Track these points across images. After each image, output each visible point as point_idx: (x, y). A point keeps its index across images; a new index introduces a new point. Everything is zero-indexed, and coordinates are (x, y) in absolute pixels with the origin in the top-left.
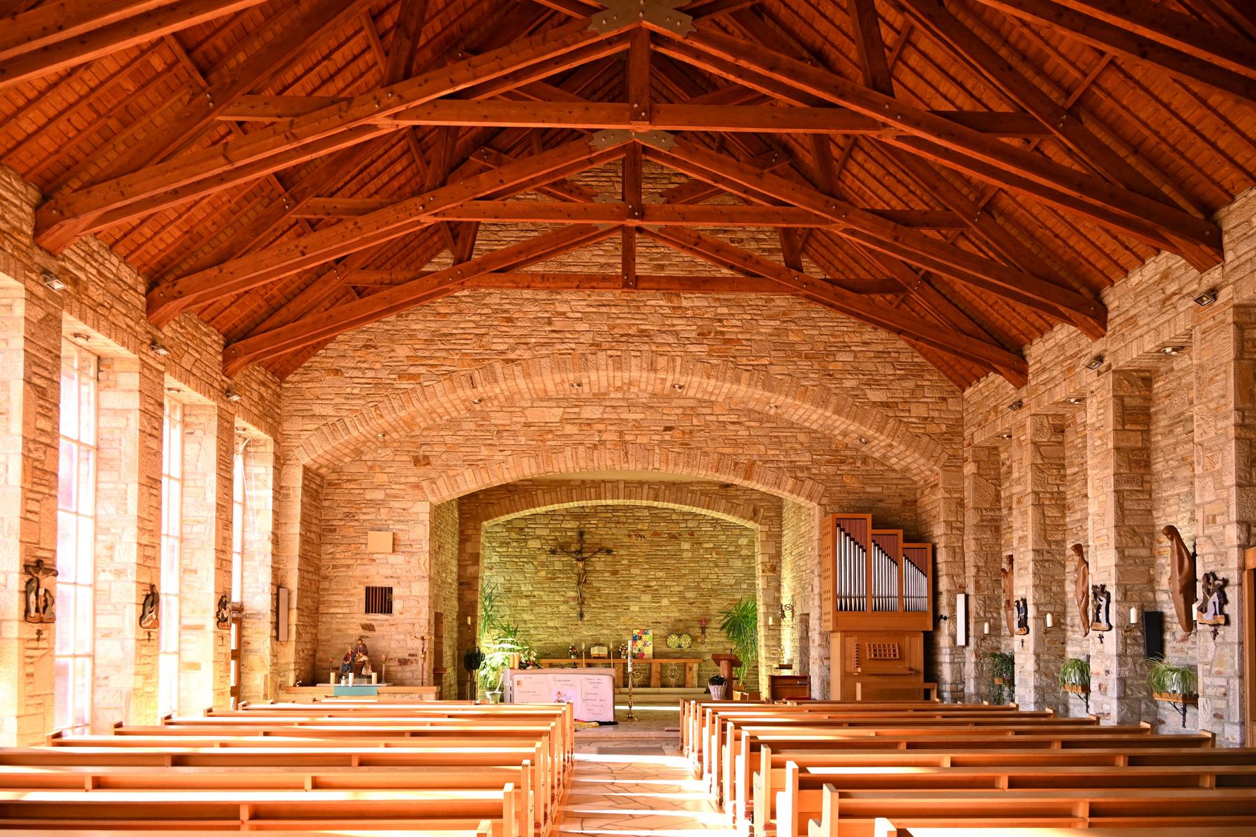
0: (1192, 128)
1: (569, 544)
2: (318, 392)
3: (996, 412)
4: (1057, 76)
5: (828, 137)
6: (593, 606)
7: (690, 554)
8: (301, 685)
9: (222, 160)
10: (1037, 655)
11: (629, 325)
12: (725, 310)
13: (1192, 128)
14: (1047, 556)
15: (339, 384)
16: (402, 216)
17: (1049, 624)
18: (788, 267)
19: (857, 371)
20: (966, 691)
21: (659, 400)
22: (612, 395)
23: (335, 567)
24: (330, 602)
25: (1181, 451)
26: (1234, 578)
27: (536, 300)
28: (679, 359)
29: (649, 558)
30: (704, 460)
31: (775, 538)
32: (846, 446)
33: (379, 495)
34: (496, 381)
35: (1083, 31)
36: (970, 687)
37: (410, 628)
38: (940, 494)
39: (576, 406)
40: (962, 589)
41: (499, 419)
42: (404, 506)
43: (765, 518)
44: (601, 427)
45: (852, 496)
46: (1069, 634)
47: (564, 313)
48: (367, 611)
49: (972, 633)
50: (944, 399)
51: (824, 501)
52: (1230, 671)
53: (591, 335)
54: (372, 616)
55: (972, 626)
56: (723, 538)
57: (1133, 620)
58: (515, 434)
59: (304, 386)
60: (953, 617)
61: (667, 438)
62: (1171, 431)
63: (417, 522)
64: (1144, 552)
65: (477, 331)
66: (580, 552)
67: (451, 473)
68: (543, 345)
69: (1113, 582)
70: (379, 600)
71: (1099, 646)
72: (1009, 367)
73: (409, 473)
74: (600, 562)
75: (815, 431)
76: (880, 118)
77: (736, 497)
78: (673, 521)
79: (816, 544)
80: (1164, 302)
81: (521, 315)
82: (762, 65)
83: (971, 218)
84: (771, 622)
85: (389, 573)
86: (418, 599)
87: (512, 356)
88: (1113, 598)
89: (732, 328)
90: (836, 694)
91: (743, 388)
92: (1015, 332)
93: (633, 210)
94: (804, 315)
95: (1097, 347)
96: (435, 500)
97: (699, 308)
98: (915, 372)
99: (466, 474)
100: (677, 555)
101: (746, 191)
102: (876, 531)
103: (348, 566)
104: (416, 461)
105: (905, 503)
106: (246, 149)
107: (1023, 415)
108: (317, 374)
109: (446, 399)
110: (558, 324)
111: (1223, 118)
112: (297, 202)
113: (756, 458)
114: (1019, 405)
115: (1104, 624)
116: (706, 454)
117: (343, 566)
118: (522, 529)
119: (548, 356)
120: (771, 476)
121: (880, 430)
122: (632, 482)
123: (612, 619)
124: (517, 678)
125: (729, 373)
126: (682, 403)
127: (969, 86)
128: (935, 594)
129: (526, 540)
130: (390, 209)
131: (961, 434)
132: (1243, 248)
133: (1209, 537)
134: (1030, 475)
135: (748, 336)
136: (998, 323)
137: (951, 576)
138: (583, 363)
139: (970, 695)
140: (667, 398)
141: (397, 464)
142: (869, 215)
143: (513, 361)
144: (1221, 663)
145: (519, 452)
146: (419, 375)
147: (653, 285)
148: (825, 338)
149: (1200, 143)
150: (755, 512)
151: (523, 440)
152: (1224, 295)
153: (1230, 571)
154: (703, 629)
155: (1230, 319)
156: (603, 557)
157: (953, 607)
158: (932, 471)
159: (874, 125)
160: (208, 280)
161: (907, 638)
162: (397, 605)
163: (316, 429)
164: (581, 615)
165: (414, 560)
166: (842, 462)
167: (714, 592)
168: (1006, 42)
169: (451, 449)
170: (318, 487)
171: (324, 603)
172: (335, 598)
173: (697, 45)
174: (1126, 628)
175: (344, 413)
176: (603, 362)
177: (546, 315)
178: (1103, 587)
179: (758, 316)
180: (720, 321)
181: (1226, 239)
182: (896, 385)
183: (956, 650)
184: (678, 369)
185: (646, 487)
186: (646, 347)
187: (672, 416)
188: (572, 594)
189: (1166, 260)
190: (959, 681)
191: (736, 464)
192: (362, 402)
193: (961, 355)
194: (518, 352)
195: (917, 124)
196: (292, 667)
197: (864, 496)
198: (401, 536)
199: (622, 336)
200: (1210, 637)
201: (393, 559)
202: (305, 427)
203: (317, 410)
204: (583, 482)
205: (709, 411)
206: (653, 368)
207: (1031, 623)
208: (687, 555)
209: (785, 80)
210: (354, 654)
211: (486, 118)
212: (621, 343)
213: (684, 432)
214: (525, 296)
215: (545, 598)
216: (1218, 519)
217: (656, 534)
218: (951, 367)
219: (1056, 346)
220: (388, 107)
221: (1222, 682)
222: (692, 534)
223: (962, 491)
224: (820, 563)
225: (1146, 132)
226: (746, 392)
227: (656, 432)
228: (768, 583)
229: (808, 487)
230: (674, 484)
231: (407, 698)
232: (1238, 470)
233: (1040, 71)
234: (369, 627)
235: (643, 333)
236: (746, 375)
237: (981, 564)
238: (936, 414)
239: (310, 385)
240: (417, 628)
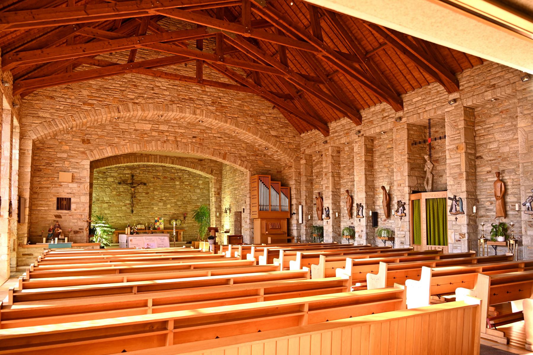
0: (401, 71)
1: (126, 180)
2: (42, 106)
3: (316, 144)
4: (365, 46)
5: (287, 48)
6: (137, 208)
7: (179, 187)
8: (30, 244)
9: (83, 12)
10: (333, 226)
11: (186, 95)
12: (222, 95)
13: (401, 71)
14: (335, 193)
15: (52, 103)
16: (129, 43)
17: (337, 216)
18: (251, 83)
19: (267, 123)
20: (302, 239)
21: (191, 125)
22: (172, 122)
23: (40, 188)
24: (38, 204)
25: (384, 163)
26: (407, 202)
27: (147, 79)
28: (205, 111)
29: (162, 187)
30: (208, 151)
31: (219, 182)
32: (259, 150)
33: (65, 155)
34: (129, 111)
35: (391, 43)
36: (303, 238)
37: (80, 217)
38: (293, 170)
39: (157, 124)
40: (300, 203)
41: (123, 126)
42: (77, 161)
43: (215, 174)
44: (167, 134)
45: (260, 168)
46: (342, 219)
47: (159, 86)
48: (58, 209)
49: (304, 219)
50: (294, 136)
51: (251, 169)
52: (406, 230)
53: (170, 97)
54: (60, 211)
55: (304, 217)
56: (193, 180)
57: (371, 214)
58: (130, 133)
59: (34, 102)
60: (298, 213)
61: (194, 141)
62: (380, 157)
63: (84, 169)
64: (372, 194)
65: (121, 89)
66: (132, 184)
67: (100, 148)
68: (150, 98)
69: (364, 202)
70: (64, 204)
71: (359, 223)
72: (324, 130)
73: (80, 146)
74: (141, 188)
75: (248, 143)
76: (320, 49)
77: (205, 165)
78: (172, 173)
79: (248, 186)
80: (383, 118)
81: (140, 84)
82: (287, 23)
83: (326, 82)
84: (218, 215)
85: (70, 191)
86: (83, 203)
87: (137, 101)
88: (364, 207)
89: (224, 101)
90: (303, 238)
91: (228, 125)
92: (326, 118)
93: (221, 58)
94: (249, 100)
95: (358, 128)
96: (92, 159)
97: (212, 92)
98: (285, 126)
99: (107, 149)
100: (174, 187)
101: (258, 58)
103: (48, 188)
104: (84, 141)
105: (278, 172)
106: (95, 10)
107: (327, 146)
108: (41, 97)
109: (104, 116)
110: (156, 91)
111: (410, 71)
112: (80, 28)
113: (227, 151)
114: (326, 142)
115: (361, 216)
116: (209, 148)
117: (45, 187)
119: (152, 103)
120: (232, 159)
121: (275, 145)
122: (163, 156)
123: (146, 213)
124: (130, 238)
125: (223, 119)
126: (200, 127)
127: (334, 41)
128: (291, 205)
129: (106, 178)
130: (124, 39)
131: (299, 149)
132: (410, 107)
133: (399, 190)
134: (330, 166)
135: (230, 106)
136: (321, 114)
137: (296, 199)
138: (167, 108)
139: (303, 241)
140: (194, 125)
141: (74, 142)
142: (298, 75)
143: (137, 103)
144: (403, 228)
145: (132, 141)
146: (94, 104)
147: (209, 84)
148: (256, 110)
149: (401, 76)
150: (212, 171)
151: (134, 136)
152: (404, 120)
153: (406, 200)
154: (185, 218)
155: (406, 127)
156: (142, 186)
157: (297, 210)
158: (289, 161)
159: (317, 50)
160: (35, 55)
162: (73, 206)
163: (40, 123)
164: (132, 211)
165: (82, 186)
166: (257, 155)
167: (189, 202)
168: (351, 33)
169: (100, 137)
170: (38, 148)
171: (34, 205)
172: (40, 202)
173: (267, 11)
174: (368, 217)
175: (55, 117)
176: (175, 109)
177: (151, 86)
178: (361, 204)
179: (234, 99)
180: (220, 98)
181: (404, 104)
182: (280, 130)
183: (298, 225)
184: (204, 115)
185: (169, 158)
186: (192, 105)
187: (196, 132)
188: (128, 202)
189: (384, 105)
190: (299, 236)
191: (220, 153)
192: (64, 113)
193: (309, 123)
194: (139, 100)
195: (330, 54)
196: (26, 235)
197: (264, 169)
198: (75, 174)
199: (183, 99)
200: (399, 220)
201: (71, 185)
202: (34, 122)
203: (41, 114)
204: (142, 154)
205: (210, 132)
206: (194, 113)
207: (331, 215)
208: (178, 187)
209: (293, 30)
210: (54, 229)
211: (193, 19)
212: (182, 102)
213: (200, 139)
214: (142, 77)
215: (115, 203)
216: (402, 185)
217: (165, 178)
218: (298, 126)
219: (341, 125)
220: (157, 7)
221: (404, 233)
222: (180, 178)
223: (300, 169)
224: (250, 193)
225: (387, 69)
226: (228, 126)
227: (190, 138)
228: (217, 199)
230: (180, 158)
231: (86, 248)
232: (408, 171)
233: (360, 44)
234: (59, 217)
235: (191, 99)
236: (229, 120)
237: (307, 195)
238: (292, 141)
239: (37, 102)
240: (83, 217)
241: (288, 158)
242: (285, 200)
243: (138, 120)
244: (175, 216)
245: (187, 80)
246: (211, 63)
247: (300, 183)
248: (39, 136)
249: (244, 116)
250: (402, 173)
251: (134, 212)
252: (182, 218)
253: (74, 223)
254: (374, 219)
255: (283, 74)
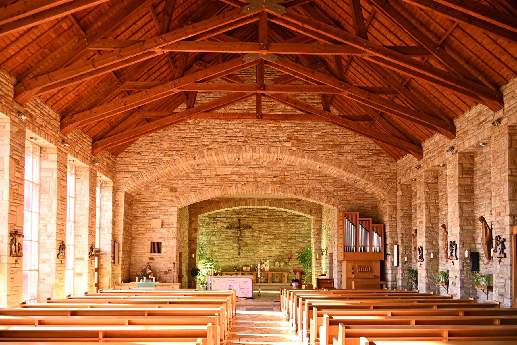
0: (491, 53)
1: (234, 224)
2: (131, 161)
3: (410, 170)
6: (244, 250)
7: (284, 229)
8: (124, 282)
10: (427, 270)
11: (259, 134)
12: (298, 128)
13: (491, 53)
14: (431, 229)
15: (139, 158)
16: (165, 89)
17: (432, 257)
18: (324, 110)
19: (353, 153)
20: (398, 285)
21: (271, 165)
22: (252, 163)
23: (138, 234)
24: (136, 248)
25: (486, 186)
26: (508, 238)
27: (221, 124)
28: (279, 148)
30: (290, 190)
31: (319, 222)
32: (348, 184)
33: (156, 204)
34: (204, 157)
35: (446, 13)
36: (399, 283)
37: (169, 259)
38: (387, 203)
39: (237, 167)
40: (396, 243)
41: (205, 173)
42: (166, 209)
43: (315, 213)
44: (248, 176)
45: (351, 205)
46: (440, 261)
47: (232, 129)
48: (151, 252)
49: (400, 261)
50: (389, 165)
51: (339, 206)
52: (506, 277)
53: (243, 138)
54: (153, 254)
55: (400, 258)
56: (298, 222)
58: (212, 179)
59: (125, 159)
60: (392, 254)
61: (275, 180)
62: (482, 178)
63: (172, 215)
64: (471, 228)
65: (196, 137)
66: (239, 227)
67: (186, 195)
68: (223, 142)
69: (458, 240)
70: (156, 247)
71: (452, 266)
72: (415, 151)
73: (169, 195)
74: (247, 232)
75: (336, 178)
76: (362, 49)
77: (303, 205)
78: (277, 215)
79: (336, 224)
80: (479, 124)
81: (214, 130)
83: (400, 90)
84: (317, 256)
85: (160, 236)
87: (211, 147)
88: (458, 246)
89: (301, 135)
91: (306, 160)
92: (418, 137)
93: (261, 87)
94: (331, 130)
95: (452, 143)
96: (179, 206)
97: (288, 127)
98: (377, 153)
99: (192, 196)
100: (279, 229)
101: (307, 79)
102: (360, 219)
103: (143, 233)
104: (171, 190)
105: (372, 207)
106: (101, 61)
107: (421, 171)
108: (131, 154)
109: (184, 164)
110: (230, 133)
111: (503, 49)
113: (311, 189)
114: (419, 167)
115: (454, 257)
116: (291, 187)
117: (141, 233)
118: (215, 218)
119: (225, 147)
120: (317, 196)
121: (362, 177)
123: (252, 255)
125: (300, 154)
126: (281, 166)
127: (399, 36)
128: (385, 245)
129: (216, 223)
130: (161, 86)
131: (396, 179)
132: (512, 102)
133: (498, 221)
134: (424, 196)
135: (308, 139)
136: (411, 133)
138: (240, 149)
139: (399, 287)
140: (275, 164)
141: (163, 191)
142: (358, 89)
143: (211, 149)
144: (502, 273)
145: (214, 186)
146: (173, 155)
147: (269, 117)
148: (339, 139)
149: (494, 59)
150: (311, 211)
151: (215, 181)
152: (504, 122)
154: (289, 259)
155: (506, 131)
156: (248, 230)
157: (392, 250)
159: (360, 51)
160: (86, 116)
161: (373, 263)
162: (163, 249)
163: (130, 177)
164: (239, 254)
165: (170, 231)
166: (347, 190)
167: (294, 244)
168: (414, 17)
169: (186, 185)
170: (131, 201)
171: (133, 248)
172: (138, 246)
173: (287, 19)
174: (463, 259)
175: (142, 170)
176: (248, 149)
177: (225, 130)
178: (454, 242)
179: (312, 130)
180: (296, 132)
181: (505, 99)
182: (369, 159)
183: (393, 268)
184: (279, 152)
185: (266, 201)
186: (266, 143)
187: (277, 172)
188: (236, 245)
189: (480, 107)
190: (395, 281)
191: (303, 191)
192: (149, 166)
193: (395, 146)
194: (213, 145)
195: (377, 51)
196: (120, 275)
197: (356, 205)
198: (165, 221)
199: (256, 138)
200: (498, 262)
201: (162, 230)
202: (126, 176)
203: (131, 169)
204: (240, 198)
205: (292, 169)
206: (269, 152)
207: (424, 257)
208: (283, 229)
209: (323, 33)
210: (146, 270)
211: (200, 49)
213: (281, 178)
214: (216, 122)
215: (224, 246)
216: (501, 214)
217: (270, 220)
218: (392, 151)
219: (435, 143)
220: (160, 44)
221: (503, 281)
222: (285, 220)
223: (396, 203)
224: (338, 232)
225: (472, 54)
226: (307, 161)
227: (270, 178)
228: (316, 240)
229: (333, 201)
230: (277, 199)
231: (167, 288)
232: (510, 194)
233: (428, 29)
234: (152, 259)
235: (265, 137)
236: (307, 155)
237: (404, 232)
238: (385, 171)
239: (128, 159)
240: (172, 259)
241: (380, 190)
242: (377, 239)
243: (219, 165)
244: (280, 258)
245: (245, 117)
246: (270, 95)
247: (396, 218)
248: (129, 188)
249: (324, 148)
250: (501, 196)
251: (241, 254)
252: (287, 260)
253: (164, 264)
254: (474, 260)
255: (340, 91)
